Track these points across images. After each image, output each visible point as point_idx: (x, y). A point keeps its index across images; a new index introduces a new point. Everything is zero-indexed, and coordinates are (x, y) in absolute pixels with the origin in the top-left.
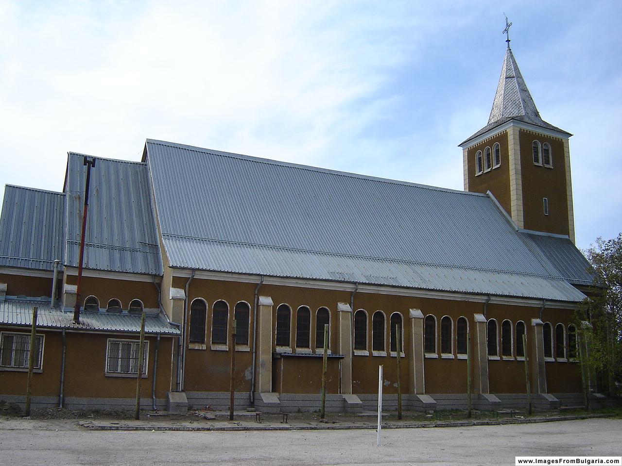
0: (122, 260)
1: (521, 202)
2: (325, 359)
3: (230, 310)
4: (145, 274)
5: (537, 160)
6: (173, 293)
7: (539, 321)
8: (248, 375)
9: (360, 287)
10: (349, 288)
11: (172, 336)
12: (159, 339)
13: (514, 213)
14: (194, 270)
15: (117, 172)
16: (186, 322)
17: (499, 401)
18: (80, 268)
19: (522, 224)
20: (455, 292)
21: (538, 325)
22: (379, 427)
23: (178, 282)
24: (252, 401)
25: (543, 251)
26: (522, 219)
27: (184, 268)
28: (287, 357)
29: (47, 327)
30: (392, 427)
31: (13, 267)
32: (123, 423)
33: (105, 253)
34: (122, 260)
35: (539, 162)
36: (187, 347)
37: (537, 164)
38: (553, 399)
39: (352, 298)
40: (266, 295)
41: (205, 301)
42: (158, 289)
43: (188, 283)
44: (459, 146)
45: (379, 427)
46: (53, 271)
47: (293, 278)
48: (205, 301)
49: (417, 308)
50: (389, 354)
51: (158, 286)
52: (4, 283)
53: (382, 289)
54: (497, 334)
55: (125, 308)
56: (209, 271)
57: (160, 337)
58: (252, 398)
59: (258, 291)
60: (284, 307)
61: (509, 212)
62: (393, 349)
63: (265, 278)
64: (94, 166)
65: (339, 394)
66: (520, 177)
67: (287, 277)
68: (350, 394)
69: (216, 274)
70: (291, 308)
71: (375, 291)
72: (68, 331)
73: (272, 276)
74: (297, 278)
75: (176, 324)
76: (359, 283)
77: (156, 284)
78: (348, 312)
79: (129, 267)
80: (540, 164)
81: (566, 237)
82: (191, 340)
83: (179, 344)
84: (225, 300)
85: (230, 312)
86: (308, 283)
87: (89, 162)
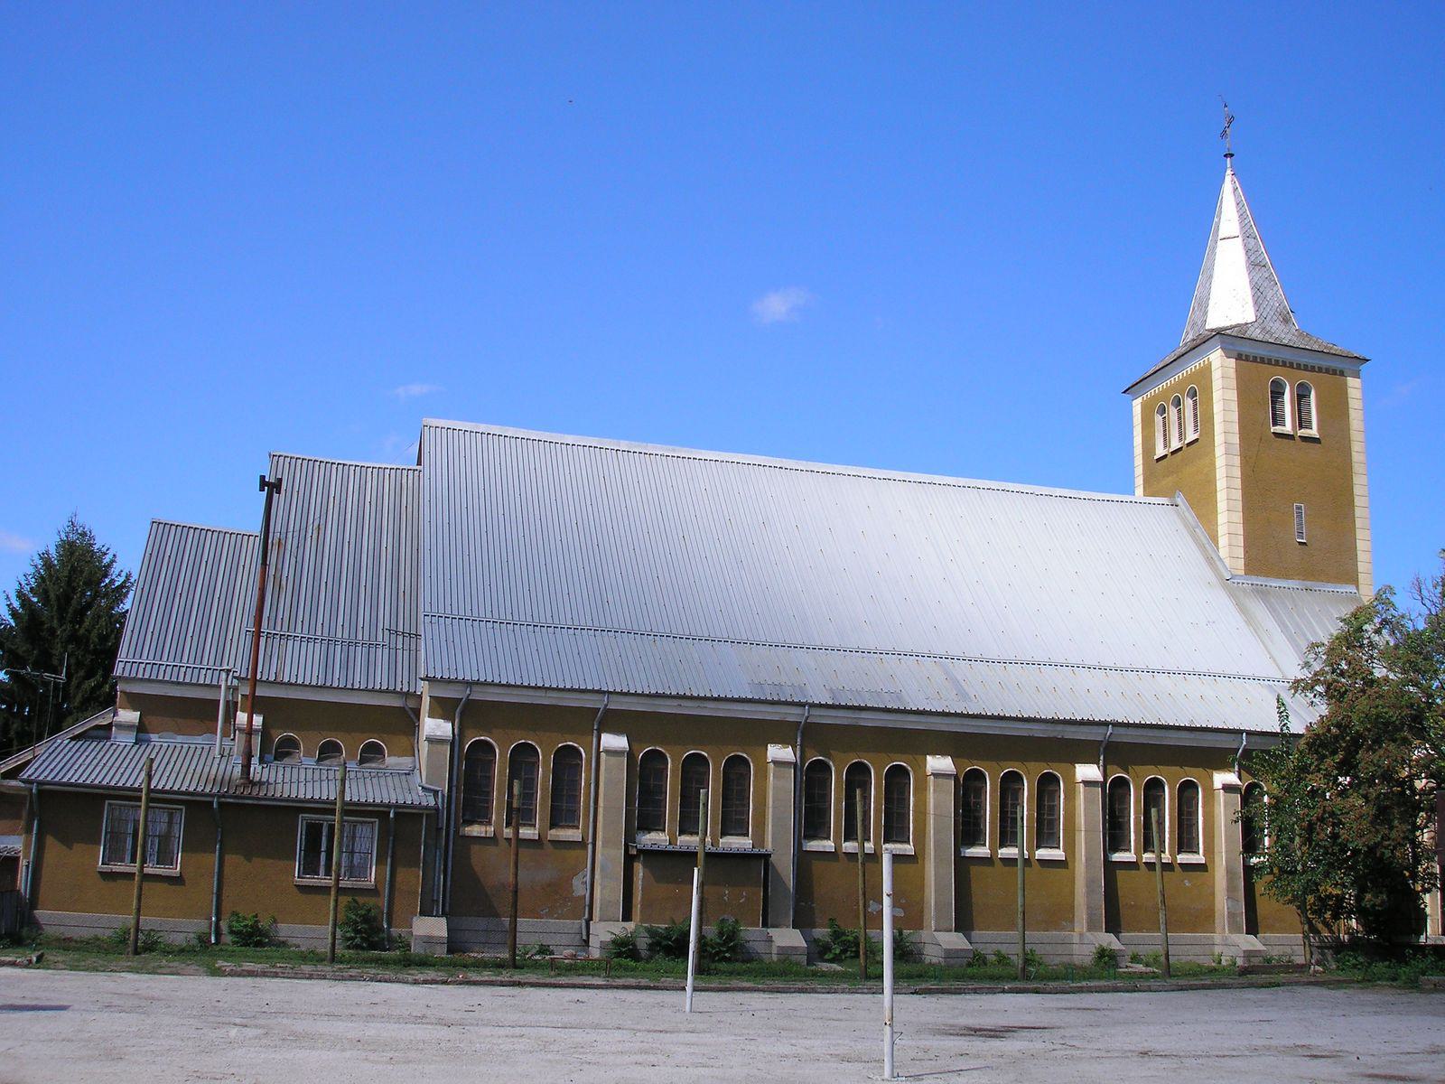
0: (347, 664)
1: (1238, 517)
2: (701, 856)
3: (586, 759)
4: (387, 691)
5: (1277, 419)
6: (434, 727)
7: (1231, 778)
8: (579, 888)
9: (815, 712)
10: (793, 715)
11: (421, 812)
12: (392, 816)
13: (1223, 541)
14: (469, 684)
15: (362, 490)
16: (455, 783)
17: (1263, 948)
18: (255, 682)
19: (1241, 563)
20: (1029, 720)
21: (1228, 788)
22: (689, 988)
23: (443, 708)
24: (584, 938)
25: (1282, 625)
26: (1240, 552)
27: (449, 681)
28: (652, 855)
29: (187, 793)
30: (819, 990)
31: (149, 680)
32: (735, 983)
33: (317, 650)
34: (347, 664)
35: (1287, 424)
36: (457, 832)
37: (1278, 429)
38: (1253, 945)
39: (799, 734)
40: (616, 731)
41: (493, 742)
42: (415, 720)
43: (458, 710)
44: (1124, 392)
45: (689, 988)
46: (220, 687)
47: (671, 697)
48: (493, 742)
49: (943, 754)
50: (838, 846)
51: (415, 713)
52: (135, 710)
53: (864, 715)
54: (859, 825)
55: (351, 756)
56: (500, 685)
57: (395, 813)
58: (584, 933)
59: (600, 723)
60: (656, 757)
61: (1214, 538)
62: (850, 836)
63: (614, 698)
64: (279, 492)
65: (760, 928)
66: (1237, 461)
67: (657, 696)
68: (951, 931)
69: (515, 691)
70: (668, 755)
71: (850, 720)
72: (223, 799)
73: (628, 694)
74: (678, 697)
75: (432, 787)
76: (813, 705)
77: (410, 712)
78: (790, 763)
79: (359, 680)
80: (1288, 428)
81: (1351, 589)
82: (467, 817)
83: (438, 825)
84: (532, 740)
85: (543, 762)
86: (702, 705)
87: (268, 484)
